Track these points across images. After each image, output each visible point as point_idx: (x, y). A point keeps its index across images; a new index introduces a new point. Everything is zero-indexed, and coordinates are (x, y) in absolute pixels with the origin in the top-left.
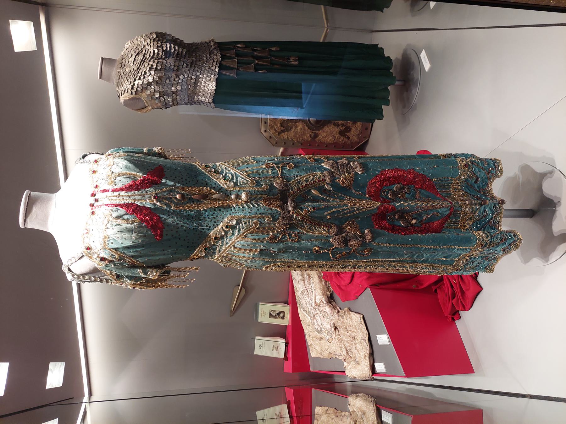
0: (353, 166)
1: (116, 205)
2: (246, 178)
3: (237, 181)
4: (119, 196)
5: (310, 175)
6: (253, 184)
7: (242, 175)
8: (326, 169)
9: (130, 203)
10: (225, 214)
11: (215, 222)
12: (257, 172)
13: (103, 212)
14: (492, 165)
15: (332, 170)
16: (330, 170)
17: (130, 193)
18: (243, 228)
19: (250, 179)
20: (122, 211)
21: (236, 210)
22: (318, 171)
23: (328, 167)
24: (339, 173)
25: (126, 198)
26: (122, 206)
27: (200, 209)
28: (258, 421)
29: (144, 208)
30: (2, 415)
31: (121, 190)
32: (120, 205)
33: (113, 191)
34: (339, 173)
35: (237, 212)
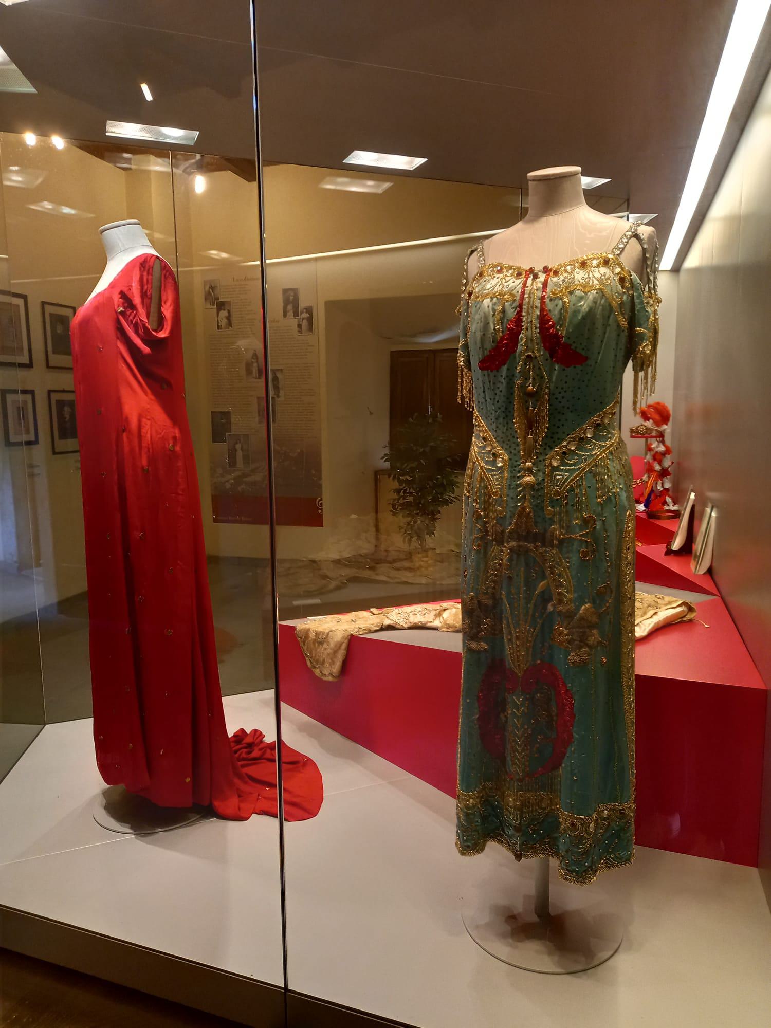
0: (581, 651)
1: (520, 306)
2: (567, 486)
3: (562, 471)
4: (533, 307)
5: (570, 582)
6: (555, 495)
7: (572, 480)
8: (578, 608)
9: (523, 324)
10: (511, 452)
11: (562, 388)
12: (578, 502)
13: (515, 284)
14: (573, 867)
15: (575, 618)
16: (575, 614)
17: (536, 323)
18: (492, 476)
19: (564, 490)
20: (511, 314)
21: (515, 467)
22: (576, 595)
23: (581, 612)
24: (570, 626)
25: (531, 318)
26: (519, 314)
27: (514, 419)
28: (266, 529)
29: (516, 342)
30: (11, 951)
31: (542, 310)
32: (521, 311)
33: (542, 298)
34: (570, 626)
35: (513, 469)
